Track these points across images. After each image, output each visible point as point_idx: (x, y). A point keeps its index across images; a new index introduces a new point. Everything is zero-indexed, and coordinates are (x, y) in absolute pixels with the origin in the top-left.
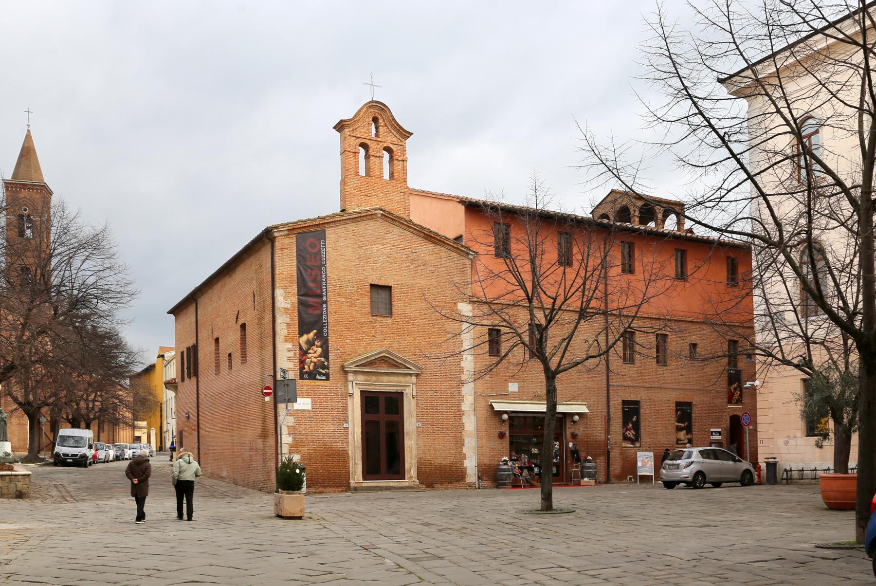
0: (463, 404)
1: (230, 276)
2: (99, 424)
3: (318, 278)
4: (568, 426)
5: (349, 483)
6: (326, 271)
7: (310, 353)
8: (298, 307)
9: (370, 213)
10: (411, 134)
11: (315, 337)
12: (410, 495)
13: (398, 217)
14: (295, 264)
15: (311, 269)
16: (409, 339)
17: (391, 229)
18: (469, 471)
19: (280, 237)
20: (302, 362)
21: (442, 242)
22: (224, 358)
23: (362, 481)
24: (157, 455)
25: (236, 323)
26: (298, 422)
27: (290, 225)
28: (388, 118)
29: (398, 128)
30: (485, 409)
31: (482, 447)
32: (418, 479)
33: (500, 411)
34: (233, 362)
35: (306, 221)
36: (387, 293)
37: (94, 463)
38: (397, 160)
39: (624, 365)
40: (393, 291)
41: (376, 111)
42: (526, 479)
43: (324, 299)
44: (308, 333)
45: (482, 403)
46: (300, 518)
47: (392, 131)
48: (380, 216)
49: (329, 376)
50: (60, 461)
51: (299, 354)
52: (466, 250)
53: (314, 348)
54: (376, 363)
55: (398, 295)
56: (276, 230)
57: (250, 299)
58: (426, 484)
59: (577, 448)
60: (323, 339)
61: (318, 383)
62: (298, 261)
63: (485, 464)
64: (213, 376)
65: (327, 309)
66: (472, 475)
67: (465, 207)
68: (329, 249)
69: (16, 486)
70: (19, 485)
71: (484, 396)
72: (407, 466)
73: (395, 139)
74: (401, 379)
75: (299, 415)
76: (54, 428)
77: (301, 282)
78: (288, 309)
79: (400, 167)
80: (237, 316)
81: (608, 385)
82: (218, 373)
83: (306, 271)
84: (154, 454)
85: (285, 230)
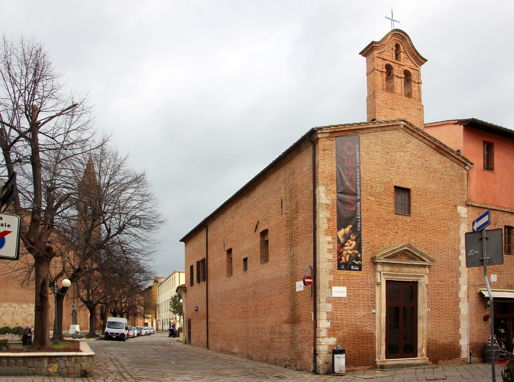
0: (460, 292)
1: (247, 197)
2: (127, 315)
5: (375, 362)
6: (360, 172)
7: (347, 246)
9: (395, 124)
11: (351, 232)
13: (417, 129)
14: (335, 164)
16: (423, 235)
17: (410, 139)
19: (322, 139)
20: (340, 254)
24: (156, 333)
26: (335, 308)
27: (332, 128)
31: (472, 328)
36: (406, 195)
37: (128, 338)
43: (358, 197)
44: (345, 227)
48: (402, 127)
49: (361, 267)
50: (109, 337)
51: (338, 247)
52: (465, 162)
53: (350, 241)
58: (433, 360)
60: (356, 232)
61: (353, 273)
63: (474, 343)
64: (242, 272)
65: (360, 206)
69: (81, 366)
70: (84, 364)
72: (419, 346)
74: (418, 270)
75: (336, 301)
76: (104, 317)
77: (340, 181)
78: (328, 205)
80: (257, 225)
84: (155, 333)
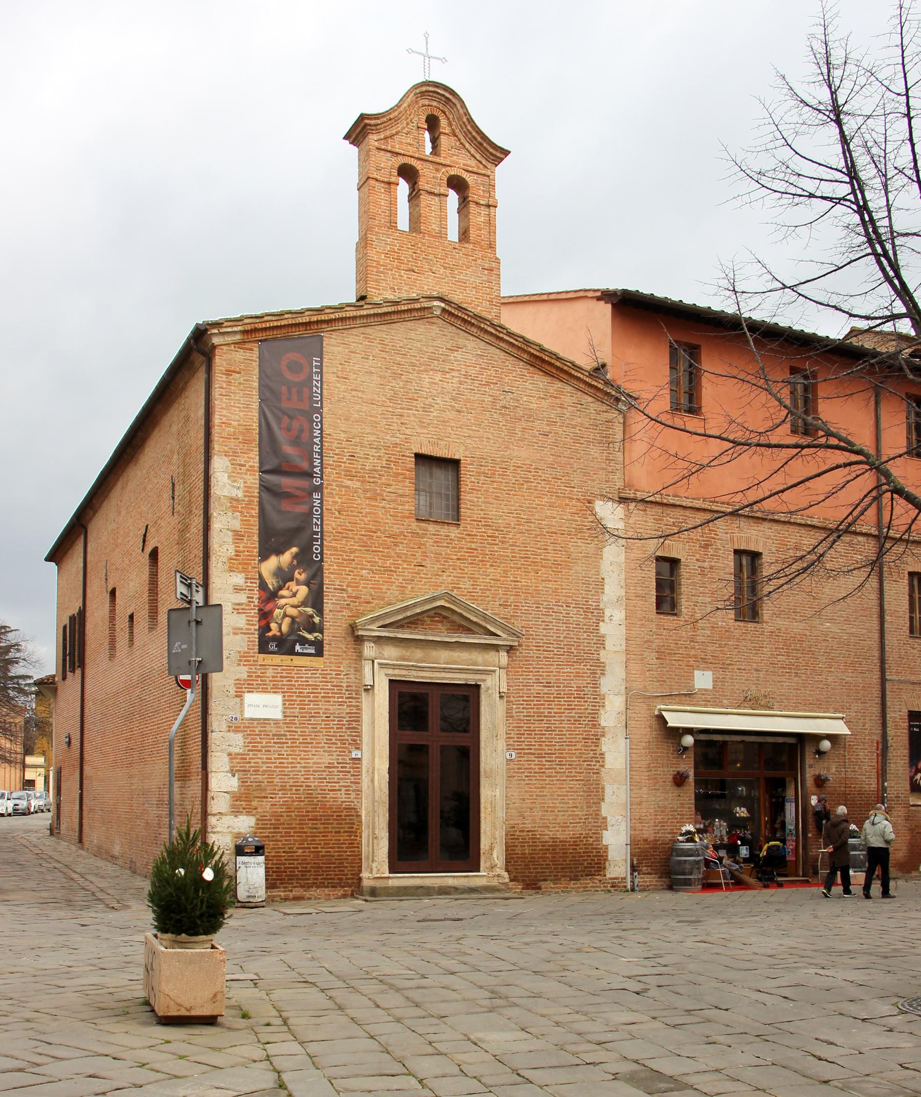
0: (602, 712)
3: (305, 436)
4: (809, 759)
5: (360, 879)
6: (321, 422)
7: (283, 597)
8: (260, 497)
9: (417, 306)
10: (506, 153)
11: (295, 562)
12: (496, 910)
13: (476, 316)
14: (256, 406)
15: (290, 417)
17: (461, 342)
18: (612, 855)
19: (225, 348)
20: (265, 616)
21: (567, 373)
22: (122, 623)
23: (387, 874)
25: (143, 550)
26: (252, 746)
27: (247, 321)
28: (460, 118)
29: (479, 139)
30: (648, 723)
31: (640, 803)
32: (507, 870)
33: (677, 729)
34: (135, 631)
35: (281, 314)
36: (450, 475)
38: (477, 203)
39: (911, 640)
40: (463, 471)
41: (435, 104)
42: (730, 872)
43: (317, 482)
44: (279, 552)
45: (642, 714)
46: (210, 1021)
47: (467, 145)
48: (438, 312)
49: (322, 647)
53: (293, 585)
54: (423, 622)
55: (473, 479)
56: (216, 331)
57: (167, 494)
58: (523, 881)
59: (828, 807)
61: (298, 661)
62: (262, 400)
63: (645, 840)
65: (321, 503)
67: (614, 305)
68: (328, 377)
71: (645, 697)
72: (484, 843)
73: (473, 163)
78: (237, 500)
79: (482, 219)
80: (145, 536)
81: (883, 680)
82: (112, 656)
83: (279, 420)
85: (235, 332)
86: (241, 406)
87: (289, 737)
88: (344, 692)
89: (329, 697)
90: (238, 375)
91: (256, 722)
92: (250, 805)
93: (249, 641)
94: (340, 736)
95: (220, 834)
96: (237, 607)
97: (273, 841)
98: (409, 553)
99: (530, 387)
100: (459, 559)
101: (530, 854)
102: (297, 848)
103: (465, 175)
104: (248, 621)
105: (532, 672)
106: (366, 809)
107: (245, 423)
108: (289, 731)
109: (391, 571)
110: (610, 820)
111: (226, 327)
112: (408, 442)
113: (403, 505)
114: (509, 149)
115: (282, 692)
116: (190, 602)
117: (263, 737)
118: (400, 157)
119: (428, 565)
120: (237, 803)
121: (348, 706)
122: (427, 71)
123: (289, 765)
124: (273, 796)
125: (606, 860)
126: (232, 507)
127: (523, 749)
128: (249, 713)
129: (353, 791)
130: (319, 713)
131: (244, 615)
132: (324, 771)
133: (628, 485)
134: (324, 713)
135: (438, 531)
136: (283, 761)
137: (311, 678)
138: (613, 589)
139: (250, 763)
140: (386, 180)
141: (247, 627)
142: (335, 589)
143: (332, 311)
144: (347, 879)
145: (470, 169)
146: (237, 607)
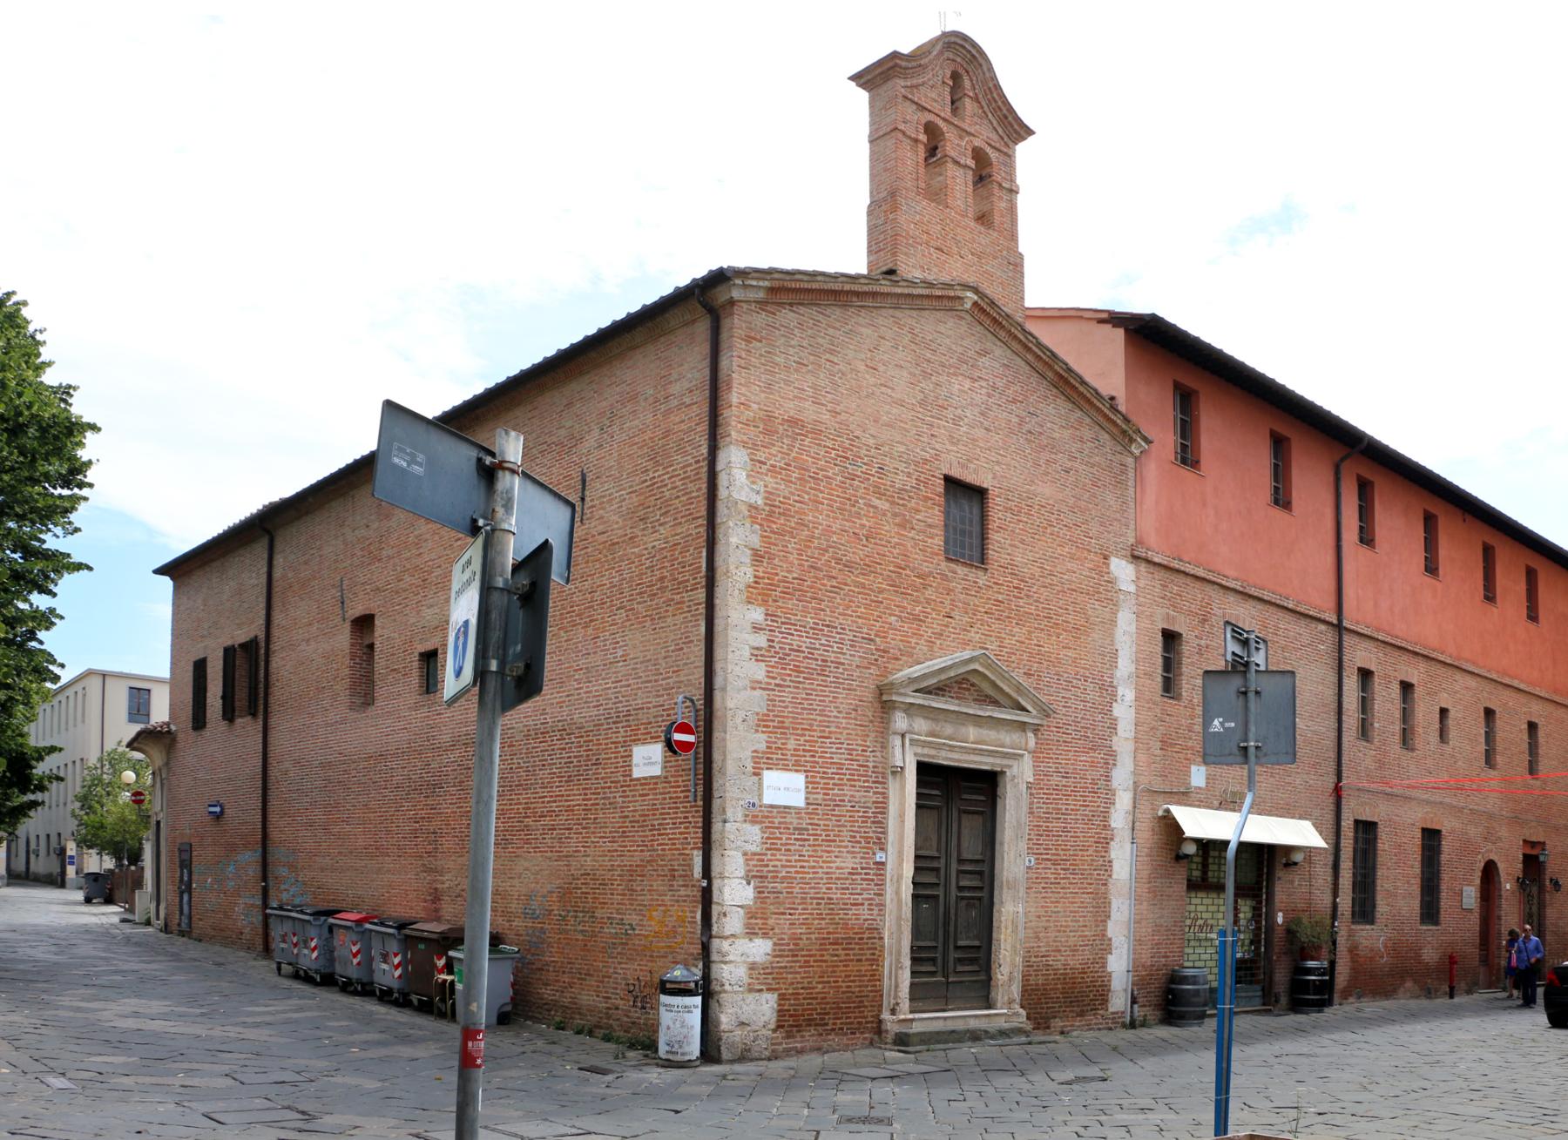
0: (1112, 810)
17: (989, 345)
19: (745, 306)
21: (1088, 401)
26: (771, 843)
27: (776, 276)
48: (968, 305)
66: (1119, 1002)
67: (1127, 331)
73: (994, 136)
78: (756, 508)
86: (762, 384)
87: (811, 832)
88: (870, 774)
89: (854, 780)
90: (759, 344)
91: (775, 810)
92: (766, 924)
93: (768, 700)
94: (865, 832)
95: (732, 965)
96: (756, 652)
97: (791, 973)
98: (938, 600)
99: (1053, 412)
100: (986, 613)
101: (1043, 984)
102: (817, 983)
103: (988, 150)
104: (768, 672)
105: (1052, 758)
106: (889, 930)
107: (765, 408)
108: (811, 824)
109: (921, 620)
110: (1115, 943)
111: (752, 279)
112: (937, 460)
113: (932, 538)
114: (1032, 127)
115: (805, 771)
116: (1247, 665)
117: (782, 830)
118: (926, 113)
119: (957, 617)
120: (753, 921)
121: (875, 793)
122: (942, 20)
123: (811, 870)
124: (792, 911)
125: (1109, 990)
126: (751, 517)
127: (1041, 854)
128: (769, 798)
129: (877, 905)
130: (844, 801)
131: (763, 664)
132: (847, 879)
133: (1139, 542)
134: (849, 801)
135: (966, 575)
136: (805, 864)
137: (836, 753)
138: (1125, 666)
139: (767, 866)
140: (913, 136)
141: (767, 680)
142: (863, 638)
143: (867, 282)
144: (867, 1023)
145: (993, 144)
146: (756, 652)
